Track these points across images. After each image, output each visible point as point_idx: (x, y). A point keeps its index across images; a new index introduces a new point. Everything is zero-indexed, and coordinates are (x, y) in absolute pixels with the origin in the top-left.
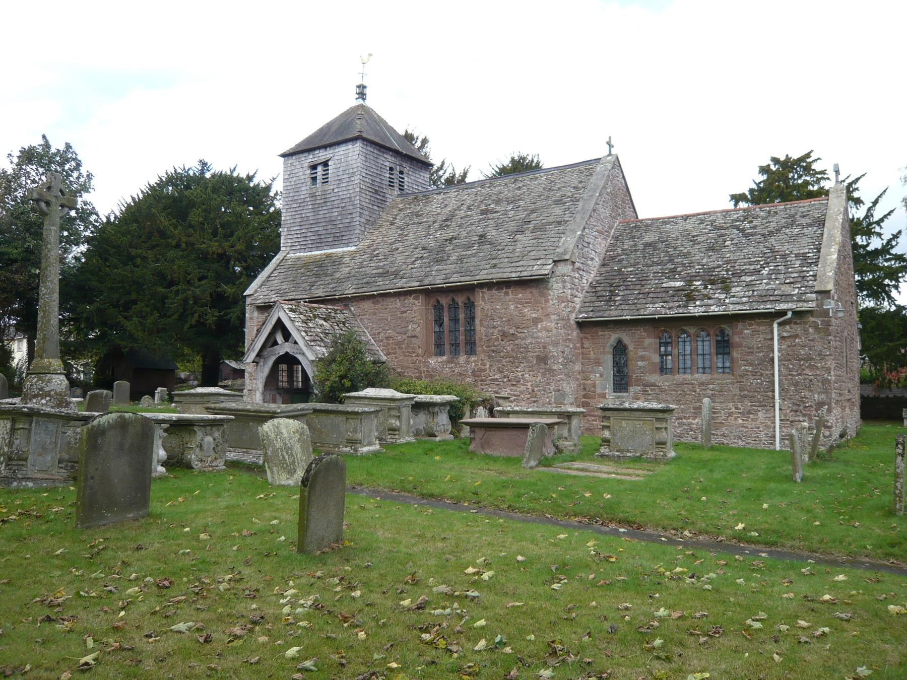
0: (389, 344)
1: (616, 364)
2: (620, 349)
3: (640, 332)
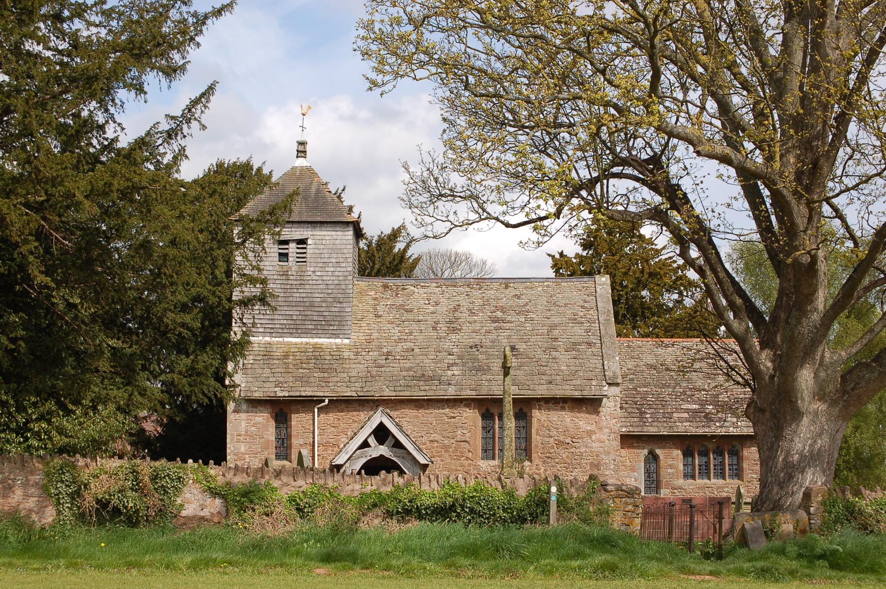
0: (433, 447)
1: (648, 472)
2: (653, 457)
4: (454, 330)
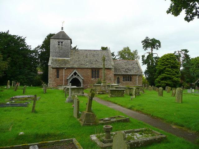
2: (118, 78)
3: (121, 76)
4: (87, 57)
